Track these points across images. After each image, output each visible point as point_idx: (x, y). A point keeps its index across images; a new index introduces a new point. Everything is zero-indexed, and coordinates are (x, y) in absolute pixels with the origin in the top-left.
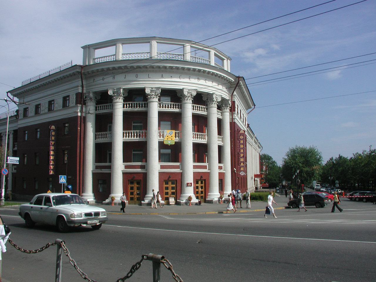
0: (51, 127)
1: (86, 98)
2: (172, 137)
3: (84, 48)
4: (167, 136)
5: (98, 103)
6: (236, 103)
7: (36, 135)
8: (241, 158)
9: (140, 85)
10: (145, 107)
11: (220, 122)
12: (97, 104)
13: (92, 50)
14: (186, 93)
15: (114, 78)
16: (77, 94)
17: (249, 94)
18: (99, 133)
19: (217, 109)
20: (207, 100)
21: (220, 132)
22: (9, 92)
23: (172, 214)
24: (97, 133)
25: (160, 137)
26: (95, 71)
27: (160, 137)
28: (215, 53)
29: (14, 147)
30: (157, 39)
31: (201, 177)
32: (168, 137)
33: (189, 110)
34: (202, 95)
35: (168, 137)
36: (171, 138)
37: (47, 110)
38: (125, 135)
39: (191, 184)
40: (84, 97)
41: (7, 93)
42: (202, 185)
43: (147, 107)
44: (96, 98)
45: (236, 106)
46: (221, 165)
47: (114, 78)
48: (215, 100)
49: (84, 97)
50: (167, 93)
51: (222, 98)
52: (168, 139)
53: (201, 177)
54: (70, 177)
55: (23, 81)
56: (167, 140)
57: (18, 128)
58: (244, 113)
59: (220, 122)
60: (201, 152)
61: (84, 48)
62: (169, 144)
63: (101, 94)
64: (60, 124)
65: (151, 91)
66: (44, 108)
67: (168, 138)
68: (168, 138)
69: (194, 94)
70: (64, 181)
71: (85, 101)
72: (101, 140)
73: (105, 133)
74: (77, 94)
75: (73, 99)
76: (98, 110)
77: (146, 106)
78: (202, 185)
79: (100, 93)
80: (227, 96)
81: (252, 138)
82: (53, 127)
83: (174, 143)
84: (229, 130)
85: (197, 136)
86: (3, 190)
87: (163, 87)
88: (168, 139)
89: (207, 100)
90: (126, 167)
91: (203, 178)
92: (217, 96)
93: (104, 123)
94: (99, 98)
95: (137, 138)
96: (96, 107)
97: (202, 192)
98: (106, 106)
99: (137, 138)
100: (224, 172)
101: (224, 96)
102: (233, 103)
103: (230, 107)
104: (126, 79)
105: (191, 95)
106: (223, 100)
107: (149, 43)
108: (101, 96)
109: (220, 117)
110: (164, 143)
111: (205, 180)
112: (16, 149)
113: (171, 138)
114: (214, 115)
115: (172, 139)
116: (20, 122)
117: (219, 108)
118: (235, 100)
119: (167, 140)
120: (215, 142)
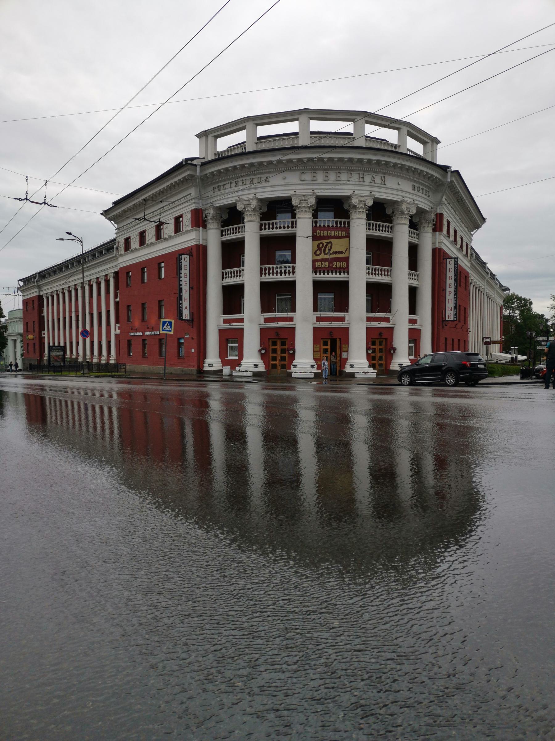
3: (198, 136)
5: (225, 223)
6: (446, 217)
9: (380, 194)
11: (413, 250)
12: (262, 219)
13: (210, 138)
17: (472, 203)
19: (409, 227)
20: (393, 213)
21: (413, 265)
25: (316, 274)
27: (316, 274)
28: (408, 131)
29: (116, 297)
31: (380, 334)
37: (154, 240)
38: (264, 272)
40: (204, 216)
42: (381, 347)
43: (296, 227)
44: (221, 217)
45: (445, 224)
46: (413, 317)
48: (406, 212)
49: (204, 216)
51: (418, 209)
53: (380, 334)
57: (120, 268)
58: (463, 236)
61: (198, 136)
65: (301, 201)
69: (370, 203)
71: (206, 221)
77: (294, 225)
78: (381, 347)
79: (228, 209)
80: (425, 205)
81: (483, 278)
84: (365, 252)
87: (319, 194)
89: (393, 213)
90: (342, 319)
91: (384, 337)
92: (409, 206)
93: (232, 254)
94: (265, 209)
95: (281, 275)
96: (222, 231)
97: (381, 358)
98: (236, 228)
99: (281, 275)
100: (420, 328)
101: (421, 206)
102: (440, 217)
103: (434, 225)
105: (365, 205)
106: (421, 212)
107: (298, 122)
108: (229, 213)
109: (415, 241)
111: (386, 339)
112: (118, 299)
114: (402, 238)
116: (121, 260)
117: (414, 225)
118: (444, 212)
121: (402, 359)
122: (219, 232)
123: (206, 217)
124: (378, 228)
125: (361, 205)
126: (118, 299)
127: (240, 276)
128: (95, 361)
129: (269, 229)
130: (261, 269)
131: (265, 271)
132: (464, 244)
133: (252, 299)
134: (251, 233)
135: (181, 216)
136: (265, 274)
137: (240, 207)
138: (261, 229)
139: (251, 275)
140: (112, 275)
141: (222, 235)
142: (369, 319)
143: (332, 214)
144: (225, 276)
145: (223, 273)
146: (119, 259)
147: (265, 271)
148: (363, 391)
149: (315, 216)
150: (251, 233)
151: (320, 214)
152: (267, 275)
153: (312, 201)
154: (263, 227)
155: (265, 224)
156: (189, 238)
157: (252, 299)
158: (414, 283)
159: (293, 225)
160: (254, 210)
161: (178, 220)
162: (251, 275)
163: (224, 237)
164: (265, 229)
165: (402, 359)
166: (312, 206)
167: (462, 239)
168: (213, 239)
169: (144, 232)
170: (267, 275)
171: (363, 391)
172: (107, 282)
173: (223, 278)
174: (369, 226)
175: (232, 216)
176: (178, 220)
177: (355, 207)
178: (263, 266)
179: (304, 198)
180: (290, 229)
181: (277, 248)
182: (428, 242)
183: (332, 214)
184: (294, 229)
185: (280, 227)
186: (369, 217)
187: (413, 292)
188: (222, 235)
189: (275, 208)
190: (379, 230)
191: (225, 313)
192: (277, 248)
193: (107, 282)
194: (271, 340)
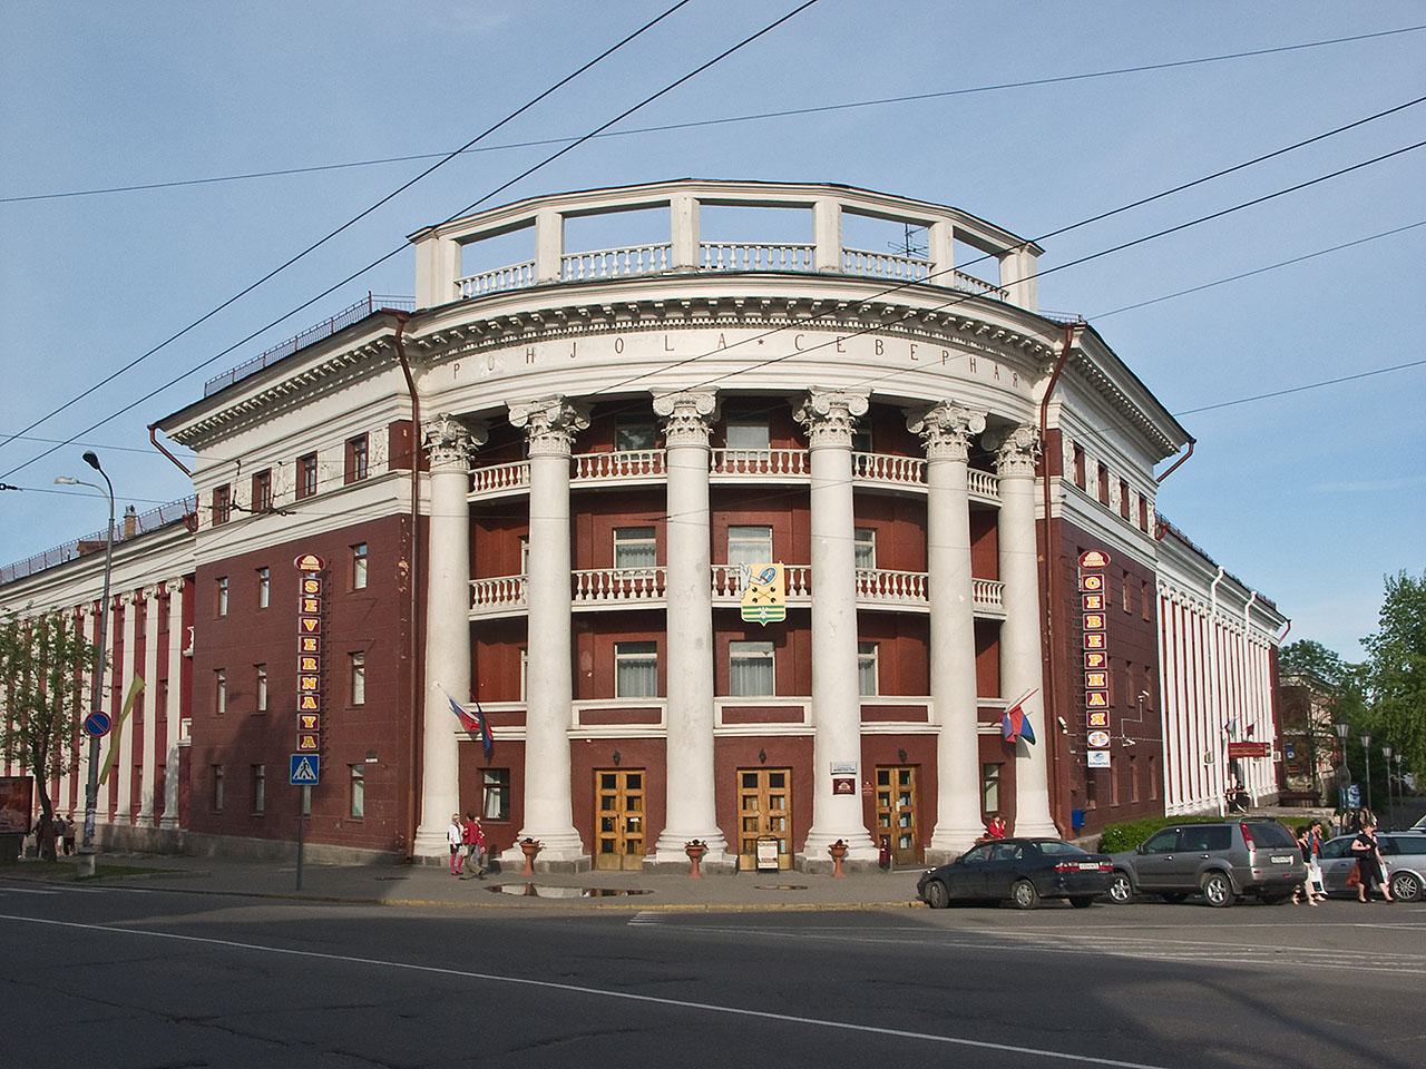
0: (300, 562)
1: (428, 440)
2: (773, 590)
4: (752, 587)
5: (480, 458)
7: (259, 601)
8: (1093, 670)
10: (657, 470)
11: (984, 521)
12: (575, 449)
14: (819, 404)
15: (530, 357)
16: (396, 428)
18: (482, 582)
19: (969, 466)
22: (158, 425)
23: (1417, 971)
24: (475, 583)
26: (422, 342)
29: (185, 644)
30: (701, 188)
31: (902, 755)
32: (755, 590)
33: (832, 474)
34: (903, 411)
35: (755, 590)
36: (772, 595)
38: (580, 587)
39: (851, 782)
41: (152, 428)
47: (530, 357)
50: (736, 409)
51: (990, 418)
52: (755, 600)
54: (372, 760)
55: (207, 380)
56: (754, 604)
59: (984, 521)
60: (896, 640)
62: (764, 620)
63: (593, 406)
64: (336, 547)
66: (284, 484)
67: (756, 595)
68: (756, 595)
69: (861, 407)
70: (307, 778)
71: (428, 451)
72: (489, 610)
73: (512, 579)
74: (396, 428)
75: (379, 447)
76: (480, 488)
82: (311, 562)
83: (784, 616)
85: (908, 585)
86: (1082, 866)
88: (755, 600)
90: (920, 714)
95: (627, 596)
96: (573, 465)
99: (627, 596)
104: (579, 360)
110: (743, 617)
112: (190, 651)
113: (772, 595)
114: (948, 486)
115: (773, 600)
119: (754, 604)
120: (952, 604)
121: (958, 826)
122: (463, 482)
123: (428, 440)
124: (885, 470)
125: (838, 414)
126: (190, 651)
127: (517, 597)
128: (101, 820)
129: (594, 474)
130: (574, 579)
131: (585, 584)
132: (1134, 500)
133: (548, 656)
134: (546, 480)
135: (363, 438)
136: (585, 593)
137: (517, 418)
138: (573, 475)
139: (546, 593)
140: (179, 584)
141: (471, 489)
142: (868, 713)
143: (763, 432)
144: (477, 597)
145: (472, 589)
146: (198, 540)
147: (585, 584)
148: (744, 673)
149: (717, 439)
150: (546, 480)
151: (731, 430)
152: (589, 596)
153: (708, 405)
154: (579, 470)
155: (584, 461)
156: (389, 496)
157: (548, 656)
158: (990, 610)
159: (661, 464)
160: (555, 426)
161: (357, 445)
162: (546, 593)
163: (476, 492)
164: (584, 474)
165: (958, 826)
166: (708, 415)
167: (1124, 485)
168: (446, 495)
169: (363, 438)
170: (589, 596)
171: (744, 673)
172: (164, 599)
173: (472, 602)
174: (859, 467)
175: (497, 439)
176: (357, 445)
177: (821, 418)
178: (580, 573)
179: (685, 396)
180: (651, 474)
181: (615, 516)
182: (1020, 499)
183: (763, 432)
184: (662, 474)
185: (620, 471)
186: (859, 443)
187: (988, 634)
188: (471, 489)
189: (618, 419)
190: (889, 476)
191: (577, 693)
192: (615, 516)
193: (164, 599)
194: (599, 775)
